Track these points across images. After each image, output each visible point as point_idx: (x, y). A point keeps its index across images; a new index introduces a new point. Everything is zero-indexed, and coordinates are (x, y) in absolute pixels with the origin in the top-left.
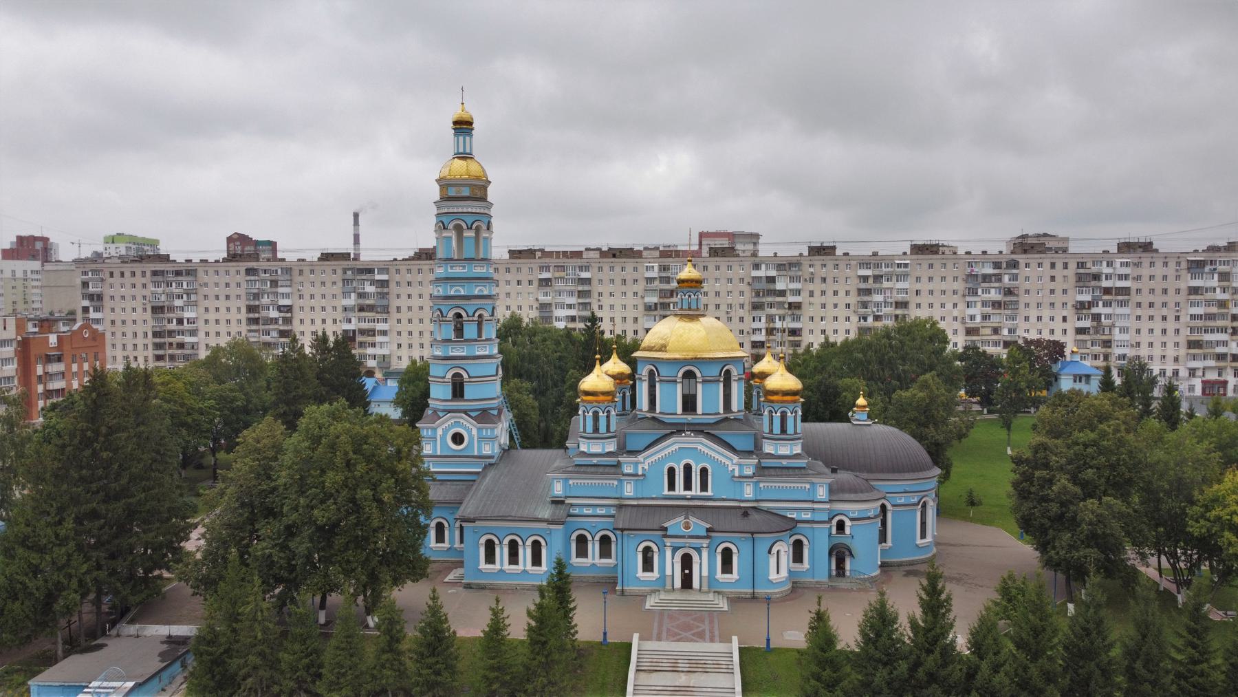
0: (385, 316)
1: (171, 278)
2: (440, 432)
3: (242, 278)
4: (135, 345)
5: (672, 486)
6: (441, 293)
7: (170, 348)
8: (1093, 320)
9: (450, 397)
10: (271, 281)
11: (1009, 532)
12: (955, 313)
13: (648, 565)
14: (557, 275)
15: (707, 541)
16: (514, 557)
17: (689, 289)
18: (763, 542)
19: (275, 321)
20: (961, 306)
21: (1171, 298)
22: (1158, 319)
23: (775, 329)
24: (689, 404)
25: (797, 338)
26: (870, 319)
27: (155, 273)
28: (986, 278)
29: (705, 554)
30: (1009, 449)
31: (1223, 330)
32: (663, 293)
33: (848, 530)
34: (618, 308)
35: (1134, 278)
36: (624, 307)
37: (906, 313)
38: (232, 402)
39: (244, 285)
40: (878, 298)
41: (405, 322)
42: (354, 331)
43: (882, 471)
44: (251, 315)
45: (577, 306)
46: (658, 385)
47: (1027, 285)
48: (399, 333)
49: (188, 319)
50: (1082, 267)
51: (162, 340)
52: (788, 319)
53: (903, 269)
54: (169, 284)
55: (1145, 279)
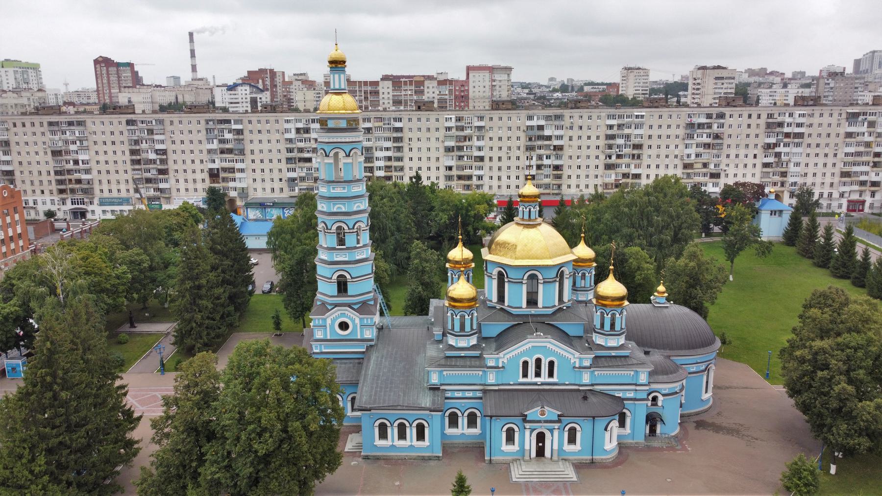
0: (242, 157)
1: (64, 127)
2: (329, 321)
3: (124, 127)
4: (41, 182)
5: (525, 375)
6: (325, 210)
7: (70, 184)
8: (776, 156)
9: (336, 294)
10: (148, 130)
11: (755, 370)
12: (677, 152)
13: (510, 439)
14: (377, 124)
15: (559, 424)
16: (402, 435)
17: (528, 204)
18: (601, 423)
19: (154, 162)
20: (681, 147)
21: (833, 140)
22: (821, 155)
23: (543, 165)
24: (532, 302)
25: (559, 172)
26: (614, 157)
27: (51, 124)
28: (700, 126)
29: (556, 433)
30: (731, 276)
31: (866, 163)
32: (459, 139)
33: (660, 403)
34: (424, 150)
35: (807, 126)
36: (429, 149)
37: (641, 152)
38: (139, 264)
39: (126, 133)
40: (620, 141)
41: (258, 161)
42: (218, 169)
43: (681, 348)
44: (134, 157)
45: (392, 149)
46: (506, 285)
47: (730, 131)
48: (254, 171)
49: (83, 161)
50: (771, 118)
51: (63, 178)
52: (553, 158)
53: (640, 120)
54: (64, 133)
55: (815, 126)
